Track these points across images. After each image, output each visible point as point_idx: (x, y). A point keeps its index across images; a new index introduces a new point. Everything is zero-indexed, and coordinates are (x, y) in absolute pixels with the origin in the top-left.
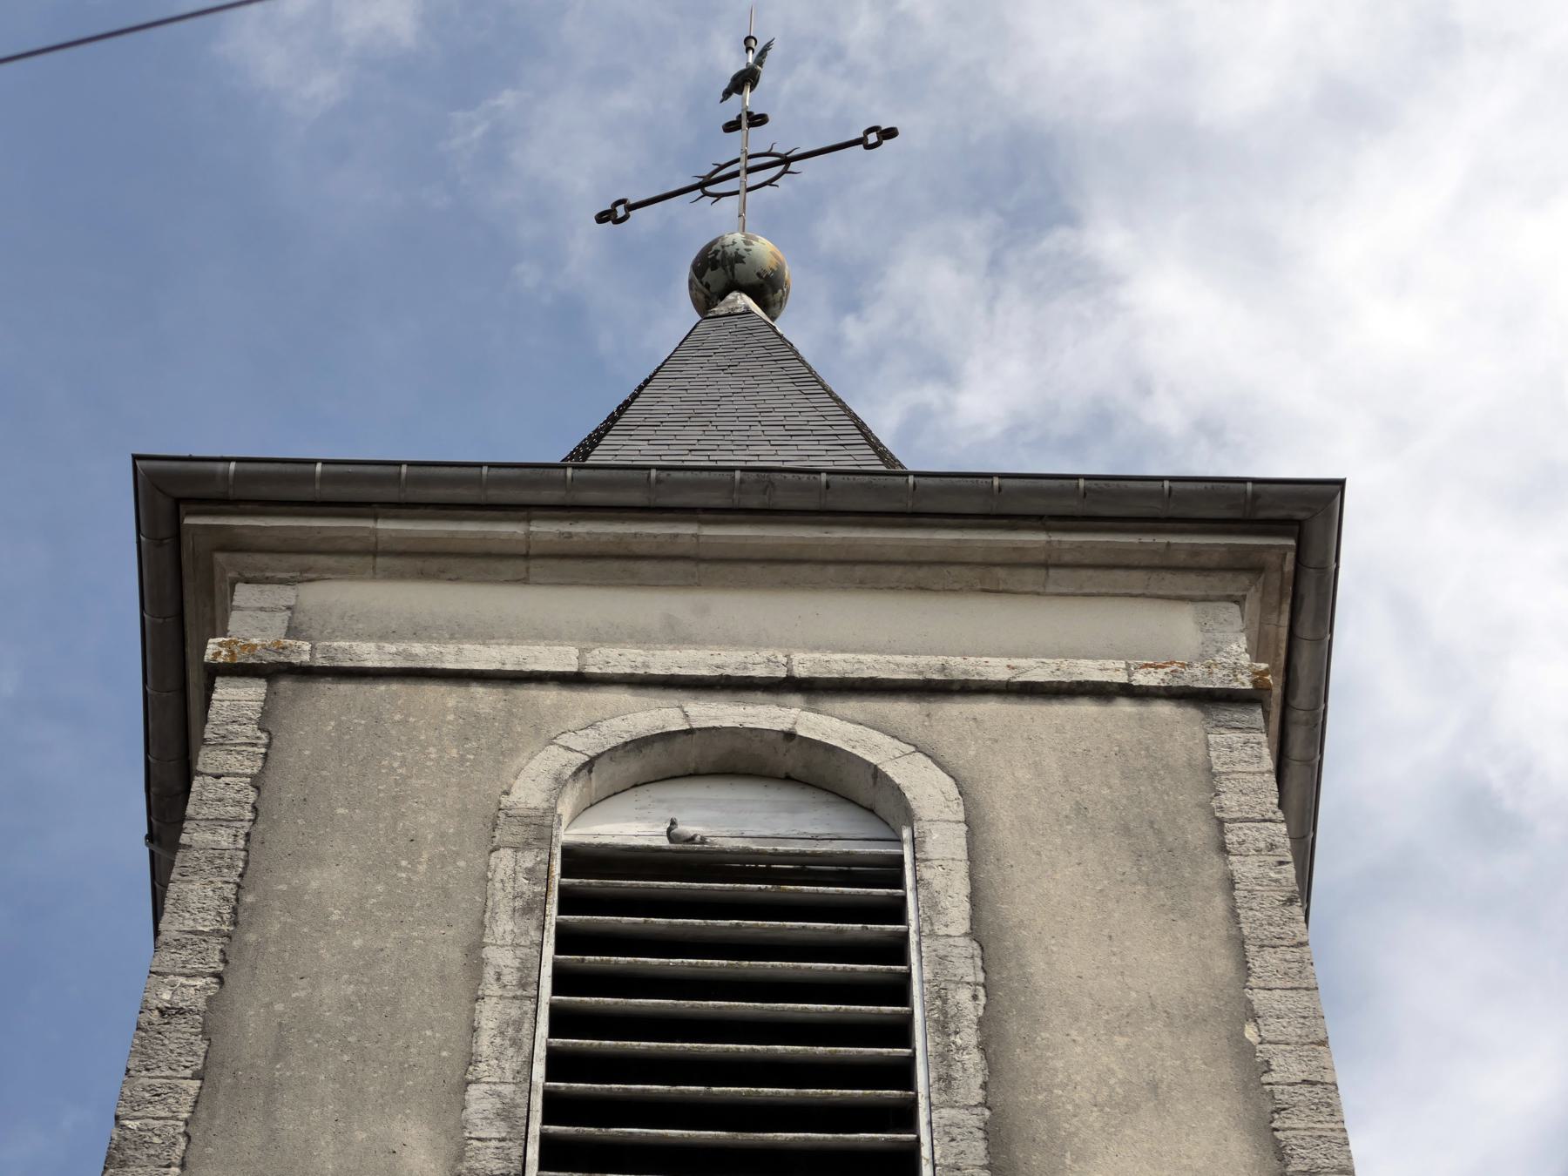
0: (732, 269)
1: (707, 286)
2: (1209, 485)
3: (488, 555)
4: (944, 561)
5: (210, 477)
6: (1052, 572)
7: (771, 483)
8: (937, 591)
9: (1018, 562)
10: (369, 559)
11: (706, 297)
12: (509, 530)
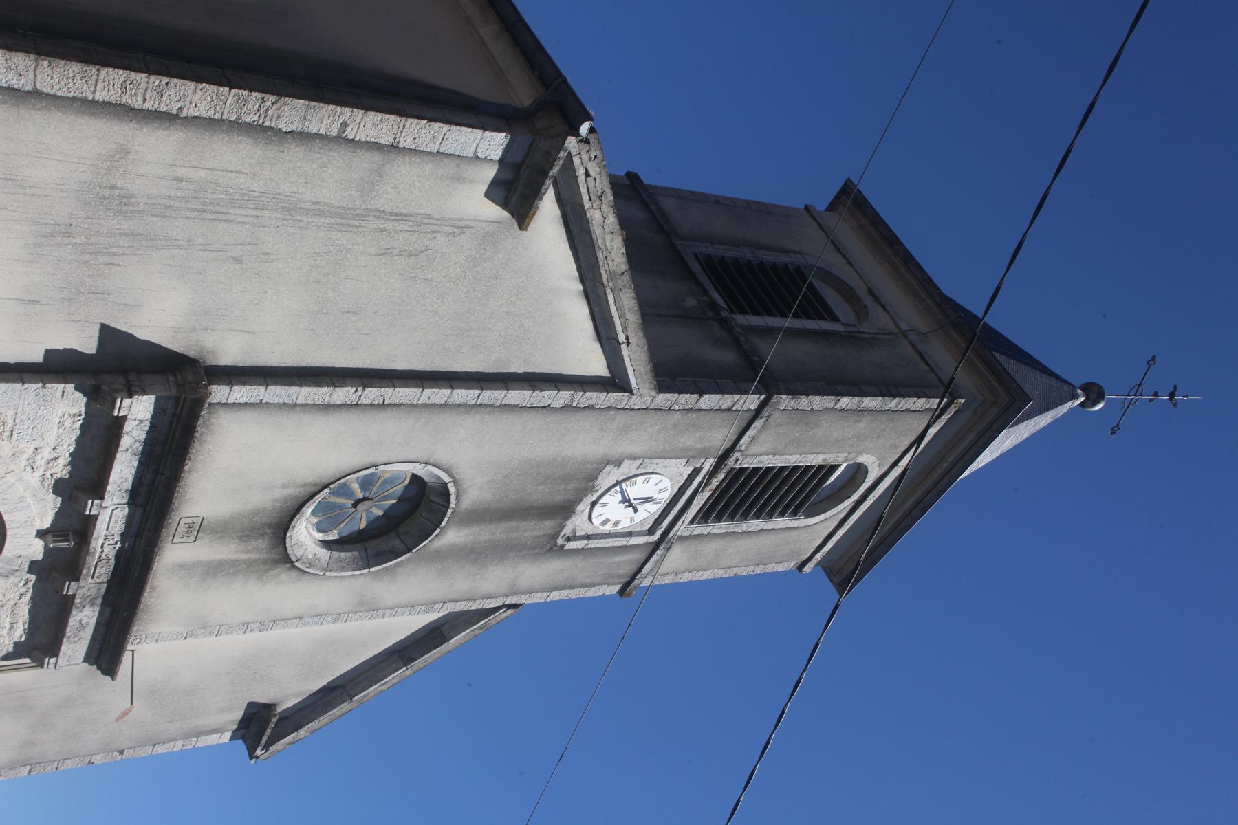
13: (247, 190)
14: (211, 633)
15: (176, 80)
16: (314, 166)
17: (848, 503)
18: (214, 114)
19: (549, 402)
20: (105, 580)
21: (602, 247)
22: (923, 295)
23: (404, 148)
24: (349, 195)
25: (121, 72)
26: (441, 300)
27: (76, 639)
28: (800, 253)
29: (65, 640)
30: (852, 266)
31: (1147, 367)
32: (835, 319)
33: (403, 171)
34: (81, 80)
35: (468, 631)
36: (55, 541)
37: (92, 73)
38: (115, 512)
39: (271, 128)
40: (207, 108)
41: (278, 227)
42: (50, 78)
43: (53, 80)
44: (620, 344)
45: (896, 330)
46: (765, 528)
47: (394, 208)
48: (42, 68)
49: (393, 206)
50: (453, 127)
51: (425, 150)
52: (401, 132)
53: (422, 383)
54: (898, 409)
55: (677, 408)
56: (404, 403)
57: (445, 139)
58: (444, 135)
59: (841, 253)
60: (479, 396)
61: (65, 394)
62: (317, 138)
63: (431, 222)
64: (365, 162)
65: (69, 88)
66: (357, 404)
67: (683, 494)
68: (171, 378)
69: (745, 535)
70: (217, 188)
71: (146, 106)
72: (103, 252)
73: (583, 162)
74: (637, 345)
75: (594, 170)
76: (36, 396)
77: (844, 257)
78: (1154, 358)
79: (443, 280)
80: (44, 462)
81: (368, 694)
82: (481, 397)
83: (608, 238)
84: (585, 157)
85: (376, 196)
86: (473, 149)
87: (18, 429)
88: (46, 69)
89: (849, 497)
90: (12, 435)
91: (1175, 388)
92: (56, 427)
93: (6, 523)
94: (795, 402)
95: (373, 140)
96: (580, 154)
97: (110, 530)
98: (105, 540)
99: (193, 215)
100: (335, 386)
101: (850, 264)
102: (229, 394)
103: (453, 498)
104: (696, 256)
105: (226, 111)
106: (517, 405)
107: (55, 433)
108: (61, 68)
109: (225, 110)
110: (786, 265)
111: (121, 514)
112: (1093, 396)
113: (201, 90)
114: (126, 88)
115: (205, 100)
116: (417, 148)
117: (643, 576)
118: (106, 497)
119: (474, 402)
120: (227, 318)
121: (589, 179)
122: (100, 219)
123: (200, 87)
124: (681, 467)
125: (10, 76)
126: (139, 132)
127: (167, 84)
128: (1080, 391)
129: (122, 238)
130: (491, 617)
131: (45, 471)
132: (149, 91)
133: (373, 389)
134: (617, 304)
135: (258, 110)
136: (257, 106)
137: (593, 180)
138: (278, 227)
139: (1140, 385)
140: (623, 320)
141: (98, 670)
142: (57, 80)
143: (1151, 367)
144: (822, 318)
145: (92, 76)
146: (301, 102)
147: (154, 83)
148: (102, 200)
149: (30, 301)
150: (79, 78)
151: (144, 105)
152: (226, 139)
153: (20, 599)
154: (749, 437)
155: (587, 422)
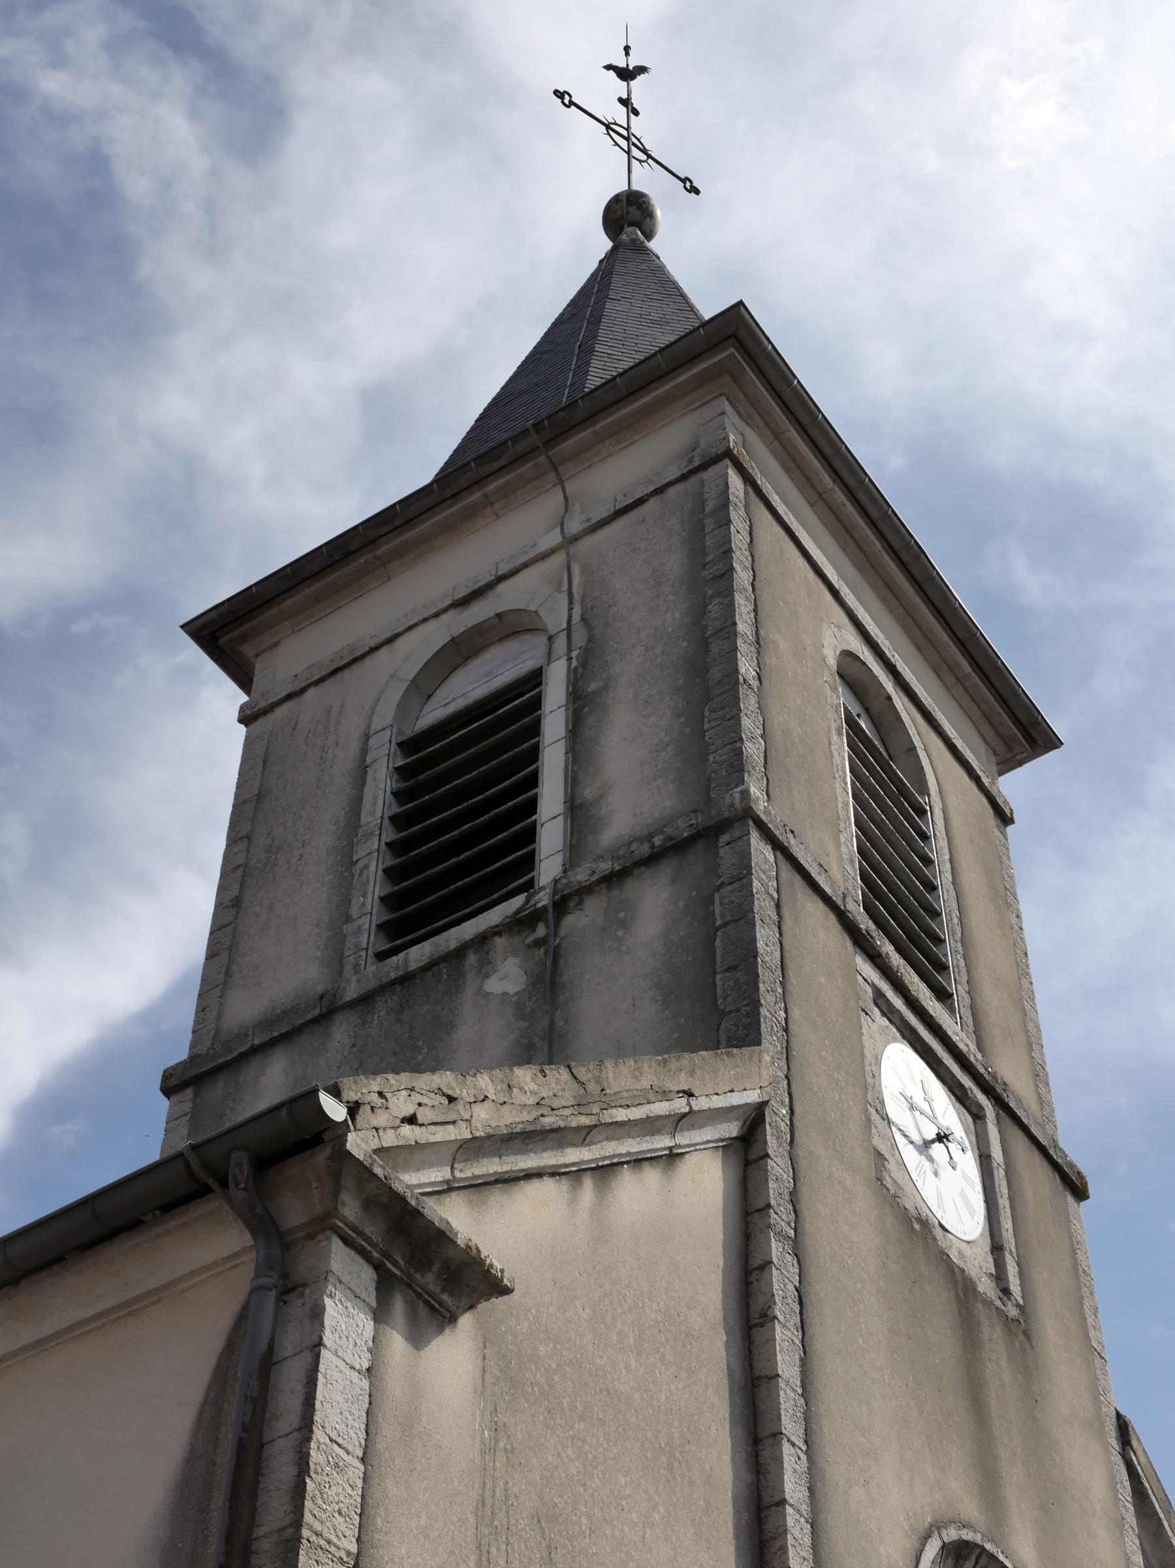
0: (645, 218)
1: (628, 213)
2: (1030, 704)
3: (808, 479)
4: (934, 645)
5: (760, 343)
6: (959, 685)
7: (919, 557)
8: (921, 654)
9: (953, 669)
10: (772, 437)
11: (622, 216)
12: (827, 480)
17: (900, 702)
19: (791, 1287)
21: (535, 1113)
22: (475, 496)
23: (357, 1541)
26: (624, 1503)
28: (366, 737)
30: (397, 636)
31: (573, 107)
32: (535, 678)
44: (691, 1111)
45: (559, 559)
46: (950, 879)
50: (318, 1417)
54: (750, 566)
55: (783, 1014)
57: (340, 1440)
58: (331, 1440)
59: (363, 657)
60: (793, 1445)
63: (488, 1501)
67: (914, 1031)
69: (963, 919)
73: (392, 1124)
74: (692, 1073)
77: (374, 649)
78: (559, 94)
82: (794, 1439)
83: (519, 1097)
84: (381, 1119)
86: (355, 1376)
89: (889, 698)
91: (609, 67)
94: (754, 768)
96: (377, 1129)
101: (390, 640)
103: (967, 1535)
104: (381, 956)
110: (397, 769)
112: (634, 213)
117: (1052, 1145)
119: (803, 1457)
121: (420, 1120)
124: (874, 1026)
128: (624, 237)
130: (1148, 1487)
134: (628, 1102)
137: (421, 1109)
139: (608, 127)
144: (536, 704)
154: (820, 874)
155: (817, 1206)
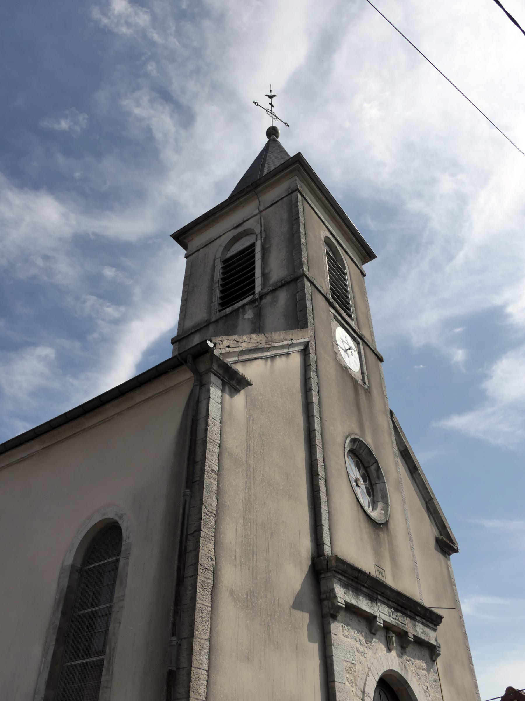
13: (243, 527)
14: (416, 566)
15: (199, 560)
16: (231, 489)
17: (339, 248)
18: (212, 540)
20: (406, 618)
22: (238, 202)
24: (241, 472)
25: (198, 590)
27: (428, 636)
28: (214, 260)
29: (430, 642)
30: (221, 236)
31: (258, 106)
33: (231, 443)
34: (203, 613)
35: (403, 437)
36: (393, 644)
37: (199, 607)
38: (380, 611)
39: (216, 511)
40: (210, 544)
41: (257, 512)
42: (203, 631)
43: (204, 629)
47: (245, 449)
48: (199, 634)
49: (244, 450)
50: (210, 413)
51: (220, 430)
52: (213, 441)
53: (313, 445)
55: (313, 321)
56: (322, 455)
57: (215, 418)
58: (213, 418)
60: (317, 417)
61: (335, 633)
62: (219, 486)
64: (227, 462)
65: (207, 621)
66: (325, 479)
68: (323, 576)
70: (243, 542)
71: (211, 578)
72: (274, 608)
74: (292, 335)
75: (226, 343)
76: (337, 649)
77: (215, 239)
79: (272, 428)
80: (362, 648)
81: (429, 488)
84: (221, 346)
85: (241, 458)
87: (351, 660)
88: (200, 633)
89: (337, 247)
90: (354, 664)
91: (266, 95)
92: (348, 639)
93: (388, 669)
95: (218, 457)
96: (220, 349)
97: (387, 614)
98: (391, 617)
99: (255, 557)
100: (319, 490)
101: (219, 237)
102: (327, 545)
103: (356, 437)
104: (220, 311)
105: (211, 534)
106: (318, 399)
107: (350, 640)
108: (198, 624)
109: (210, 534)
110: (222, 267)
111: (381, 607)
113: (203, 547)
114: (205, 588)
115: (207, 545)
116: (220, 434)
118: (376, 615)
119: (319, 420)
120: (295, 544)
122: (261, 608)
123: (202, 547)
125: (204, 653)
126: (223, 583)
127: (201, 565)
128: (271, 138)
129: (267, 597)
131: (365, 647)
132: (205, 576)
133: (319, 471)
135: (209, 516)
136: (207, 516)
138: (257, 512)
139: (267, 110)
140: (283, 340)
141: (439, 625)
142: (204, 627)
143: (259, 104)
144: (254, 251)
145: (201, 607)
146: (204, 492)
147: (201, 573)
148: (253, 606)
149: (297, 650)
150: (202, 614)
151: (211, 579)
152: (223, 535)
153: (414, 664)
155: (322, 364)
